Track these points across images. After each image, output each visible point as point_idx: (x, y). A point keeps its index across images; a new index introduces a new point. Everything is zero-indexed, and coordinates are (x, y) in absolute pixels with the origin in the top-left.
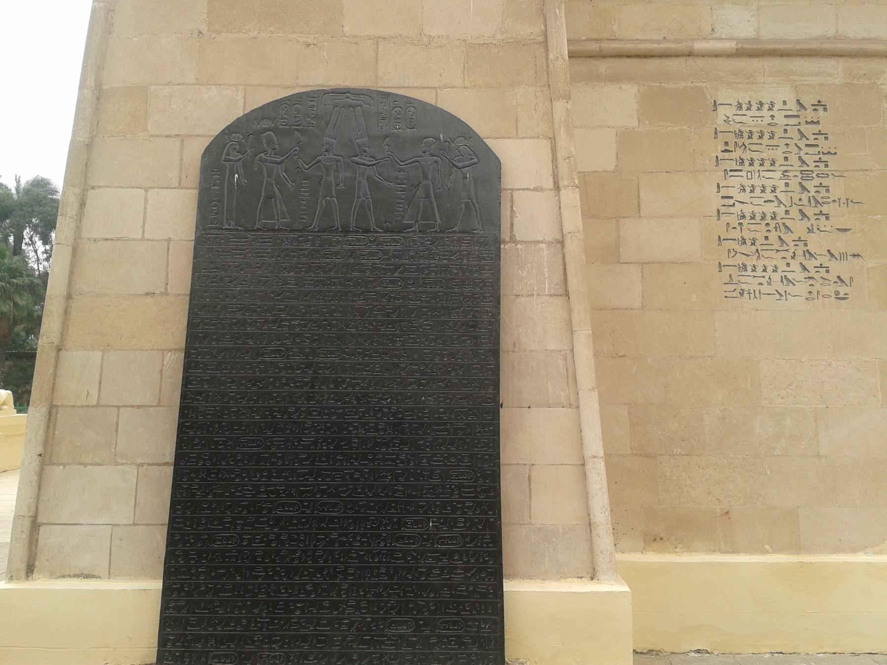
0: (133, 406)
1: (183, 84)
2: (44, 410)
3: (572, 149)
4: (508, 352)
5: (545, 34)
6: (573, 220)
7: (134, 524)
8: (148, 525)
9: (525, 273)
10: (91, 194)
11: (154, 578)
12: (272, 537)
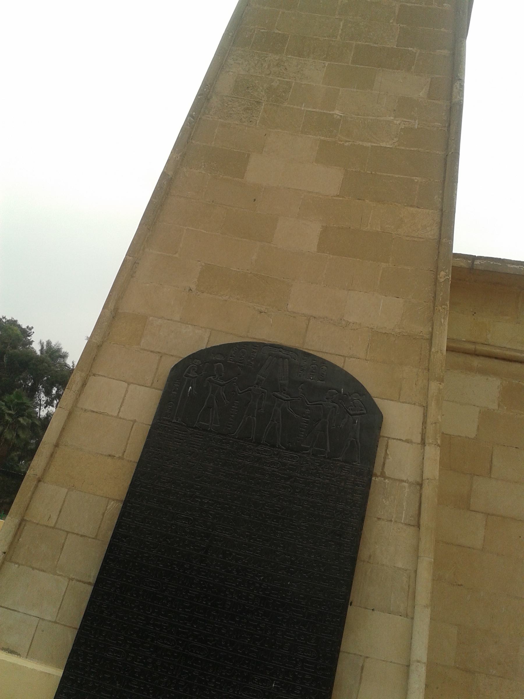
0: (77, 534)
1: (171, 320)
2: (17, 521)
3: (439, 417)
4: (364, 561)
5: (431, 334)
6: (432, 470)
7: (55, 622)
8: (65, 626)
9: (388, 502)
10: (92, 379)
11: (58, 667)
12: (150, 660)
